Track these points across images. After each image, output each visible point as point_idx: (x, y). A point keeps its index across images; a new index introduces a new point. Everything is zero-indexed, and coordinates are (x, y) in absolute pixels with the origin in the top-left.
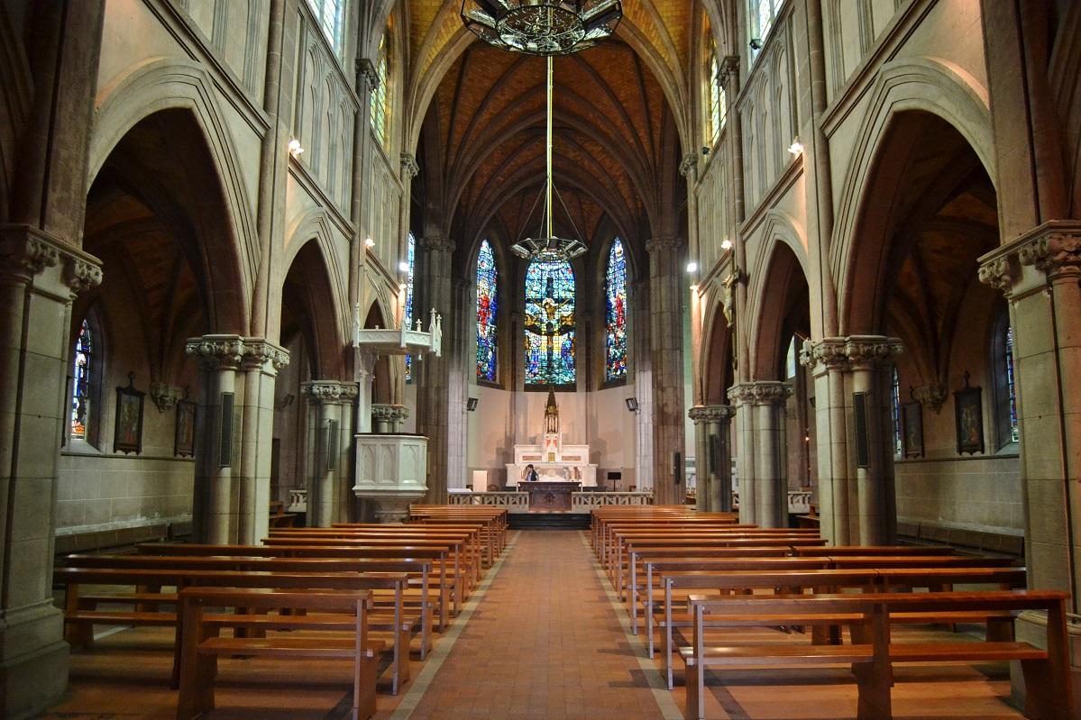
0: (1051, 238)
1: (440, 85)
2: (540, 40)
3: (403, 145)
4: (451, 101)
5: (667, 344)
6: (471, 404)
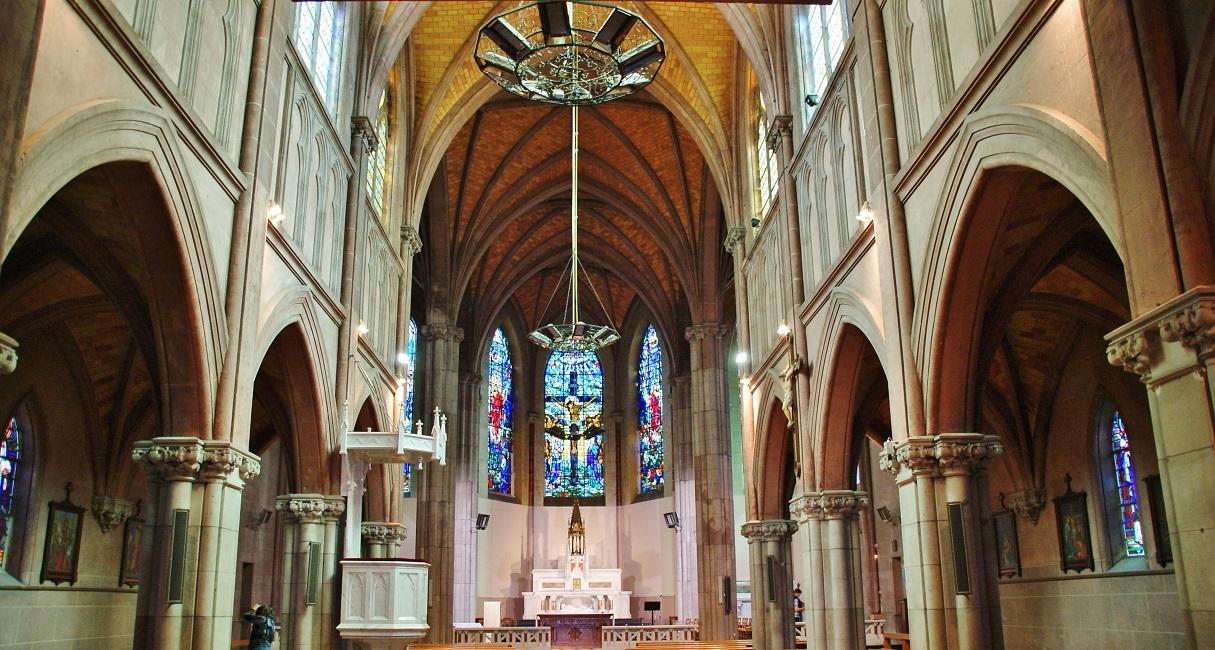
0: (1201, 307)
1: (447, 151)
2: (568, 85)
3: (405, 217)
4: (460, 168)
5: (713, 448)
6: (482, 521)
